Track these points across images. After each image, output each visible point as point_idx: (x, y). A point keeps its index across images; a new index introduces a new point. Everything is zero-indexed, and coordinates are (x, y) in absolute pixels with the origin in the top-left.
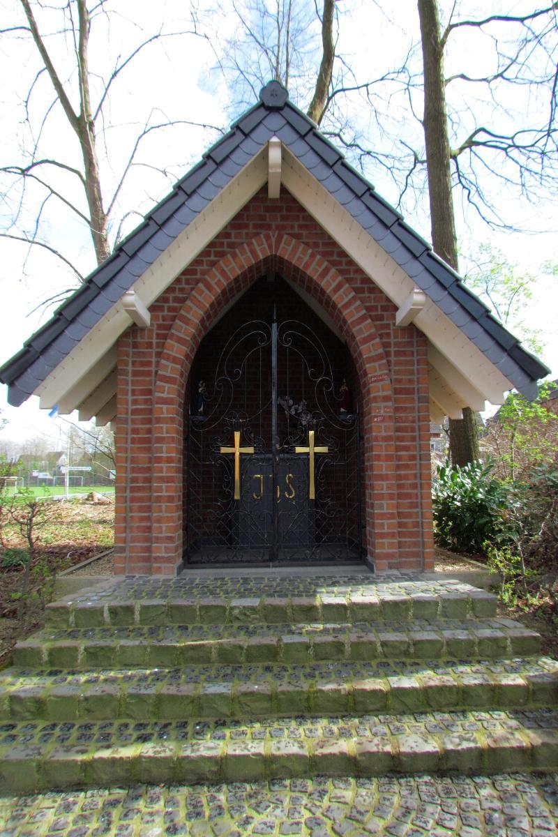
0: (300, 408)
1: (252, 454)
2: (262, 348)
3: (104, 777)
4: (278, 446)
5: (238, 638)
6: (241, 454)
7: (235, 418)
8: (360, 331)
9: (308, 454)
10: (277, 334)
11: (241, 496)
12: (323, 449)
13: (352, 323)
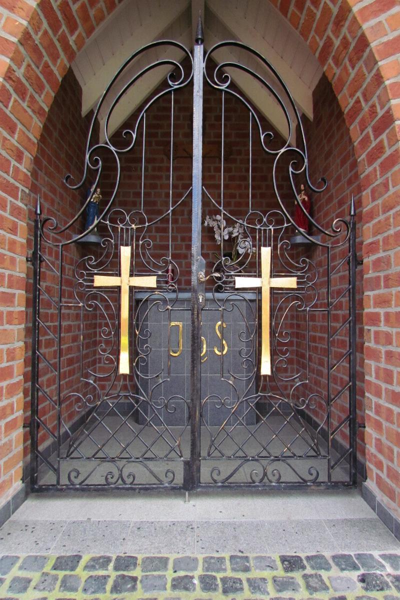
0: (236, 230)
1: (151, 289)
2: (175, 90)
3: (245, 303)
4: (202, 275)
5: (200, 257)
6: (132, 289)
7: (122, 221)
8: (379, 29)
9: (259, 290)
10: (203, 65)
11: (131, 368)
12: (289, 282)
13: (361, 11)
